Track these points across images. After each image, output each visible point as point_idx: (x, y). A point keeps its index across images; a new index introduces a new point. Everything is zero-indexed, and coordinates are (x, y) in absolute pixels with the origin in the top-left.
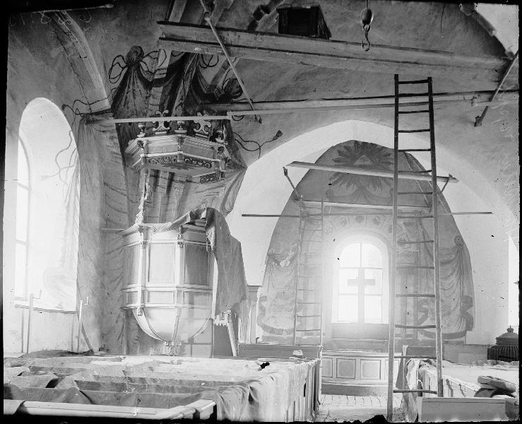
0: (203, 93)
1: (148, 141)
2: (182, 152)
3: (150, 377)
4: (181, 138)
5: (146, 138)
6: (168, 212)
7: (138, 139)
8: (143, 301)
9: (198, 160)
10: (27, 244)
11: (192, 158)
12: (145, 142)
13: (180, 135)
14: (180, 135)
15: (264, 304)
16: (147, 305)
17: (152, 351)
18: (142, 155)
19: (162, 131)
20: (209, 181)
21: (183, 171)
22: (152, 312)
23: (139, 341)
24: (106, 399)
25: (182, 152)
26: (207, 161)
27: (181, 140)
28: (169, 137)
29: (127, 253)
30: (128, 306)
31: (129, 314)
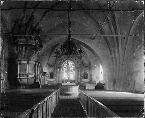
22: (23, 79)
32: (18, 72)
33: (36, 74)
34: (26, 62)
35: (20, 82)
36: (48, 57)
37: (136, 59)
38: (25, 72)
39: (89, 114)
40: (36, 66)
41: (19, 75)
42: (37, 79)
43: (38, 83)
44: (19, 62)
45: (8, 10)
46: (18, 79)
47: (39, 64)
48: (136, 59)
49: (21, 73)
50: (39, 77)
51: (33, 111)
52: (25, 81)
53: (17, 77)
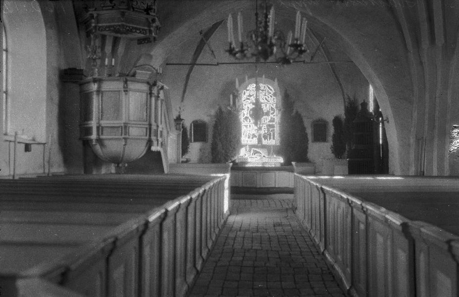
0: (115, 60)
1: (98, 14)
2: (124, 23)
3: (300, 111)
4: (123, 12)
5: (96, 12)
6: (97, 122)
7: (90, 12)
8: (98, 134)
9: (136, 29)
10: (6, 51)
11: (133, 27)
12: (95, 15)
13: (122, 10)
14: (122, 10)
15: (273, 112)
16: (102, 137)
17: (268, 24)
18: (93, 25)
19: (108, 6)
20: (145, 42)
21: (124, 36)
22: (106, 143)
23: (94, 161)
24: (220, 146)
25: (124, 23)
26: (143, 30)
27: (123, 14)
28: (113, 11)
29: (86, 99)
30: (86, 137)
31: (87, 143)
32: (91, 119)
33: (150, 125)
34: (118, 85)
35: (102, 154)
36: (185, 70)
37: (235, 166)
38: (117, 118)
39: (331, 247)
40: (151, 97)
41: (98, 128)
42: (155, 143)
43: (159, 153)
44: (94, 87)
45: (216, 65)
46: (94, 143)
47: (161, 92)
48: (235, 166)
49: (104, 123)
50: (161, 136)
51: (262, 164)
52: (114, 146)
53: (91, 134)
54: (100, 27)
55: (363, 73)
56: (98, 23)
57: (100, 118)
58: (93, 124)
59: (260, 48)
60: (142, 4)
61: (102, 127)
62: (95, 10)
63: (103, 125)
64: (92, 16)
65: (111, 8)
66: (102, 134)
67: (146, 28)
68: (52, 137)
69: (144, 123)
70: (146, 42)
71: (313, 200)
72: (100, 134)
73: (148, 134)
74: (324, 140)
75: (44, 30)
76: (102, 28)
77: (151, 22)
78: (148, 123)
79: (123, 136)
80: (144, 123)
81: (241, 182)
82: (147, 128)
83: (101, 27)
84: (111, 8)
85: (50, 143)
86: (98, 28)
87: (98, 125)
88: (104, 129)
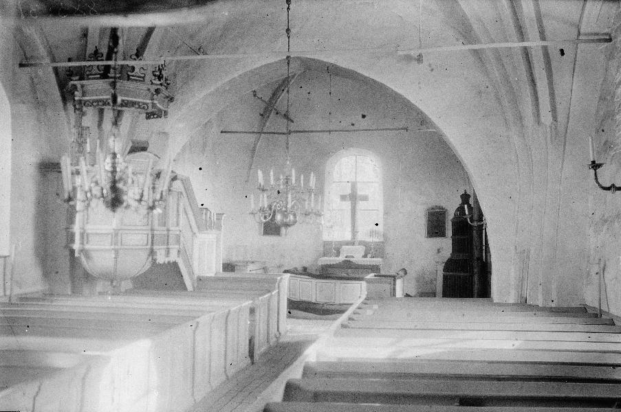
8: (82, 243)
12: (79, 86)
16: (87, 247)
22: (93, 254)
41: (82, 235)
54: (86, 101)
55: (9, 164)
56: (83, 96)
57: (85, 222)
58: (76, 229)
59: (181, 125)
60: (142, 70)
61: (88, 235)
62: (80, 79)
63: (89, 231)
64: (75, 87)
65: (99, 76)
66: (87, 243)
67: (148, 101)
68: (16, 248)
69: (144, 228)
70: (155, 116)
71: (198, 349)
72: (85, 242)
73: (150, 241)
74: (443, 234)
75: (8, 106)
76: (88, 103)
77: (154, 93)
78: (149, 227)
79: (112, 247)
80: (144, 228)
81: (314, 297)
82: (148, 235)
83: (88, 101)
84: (99, 76)
85: (13, 255)
86: (83, 102)
87: (82, 231)
88: (91, 235)
